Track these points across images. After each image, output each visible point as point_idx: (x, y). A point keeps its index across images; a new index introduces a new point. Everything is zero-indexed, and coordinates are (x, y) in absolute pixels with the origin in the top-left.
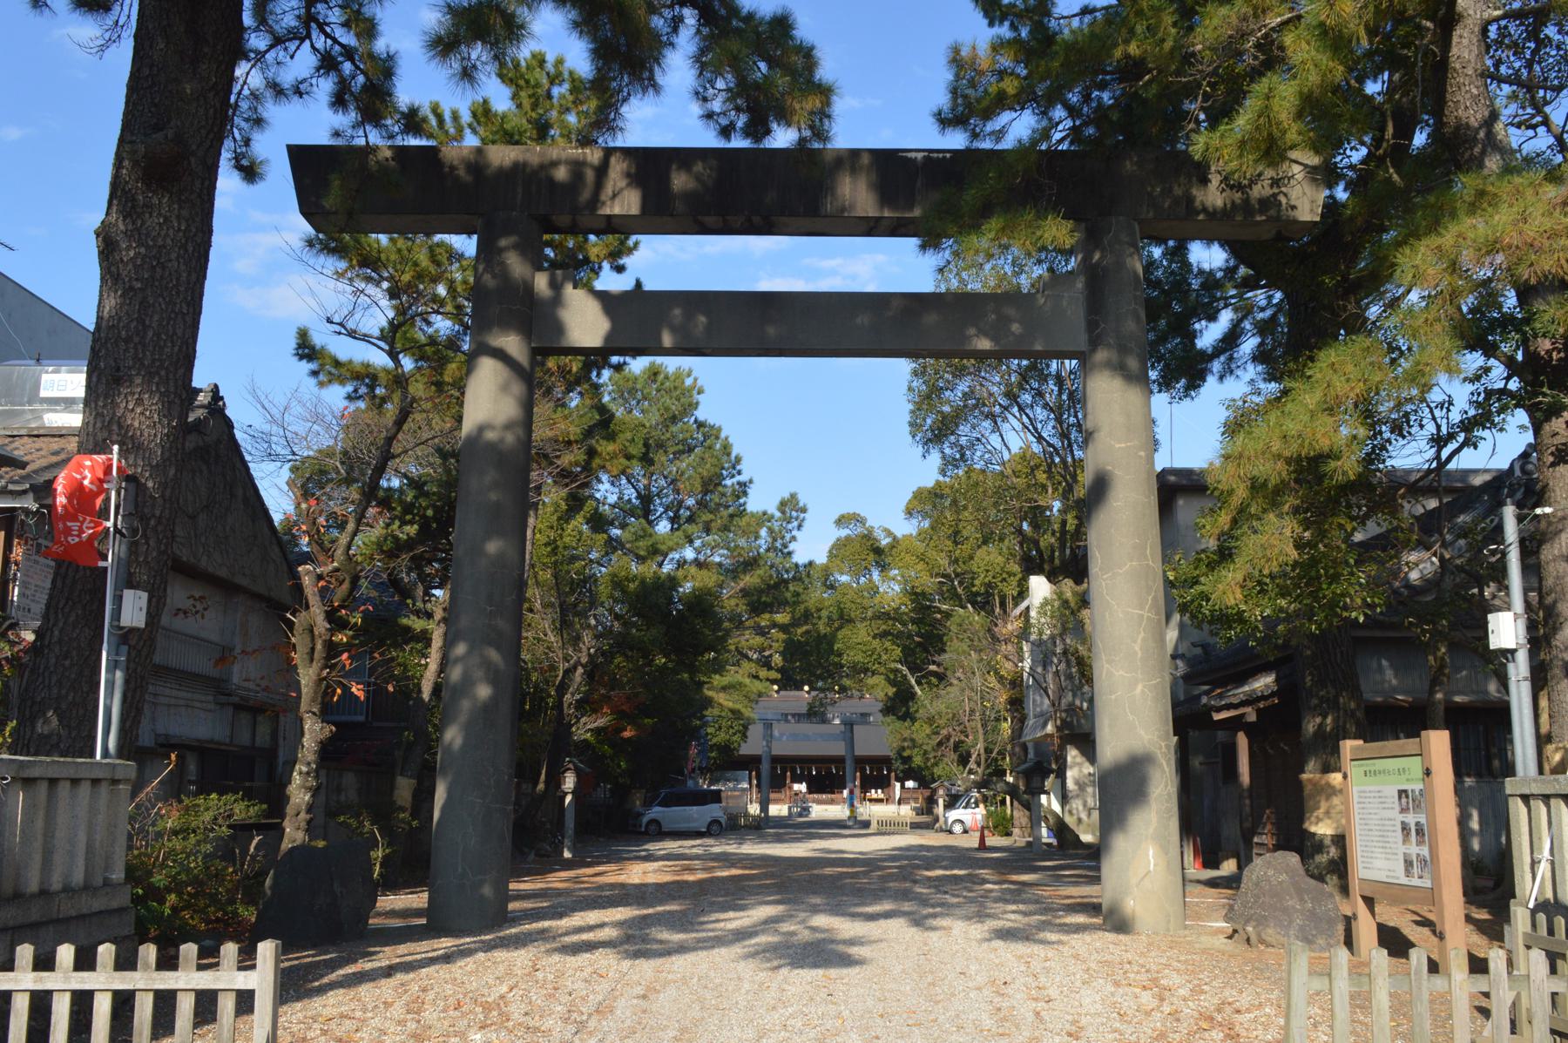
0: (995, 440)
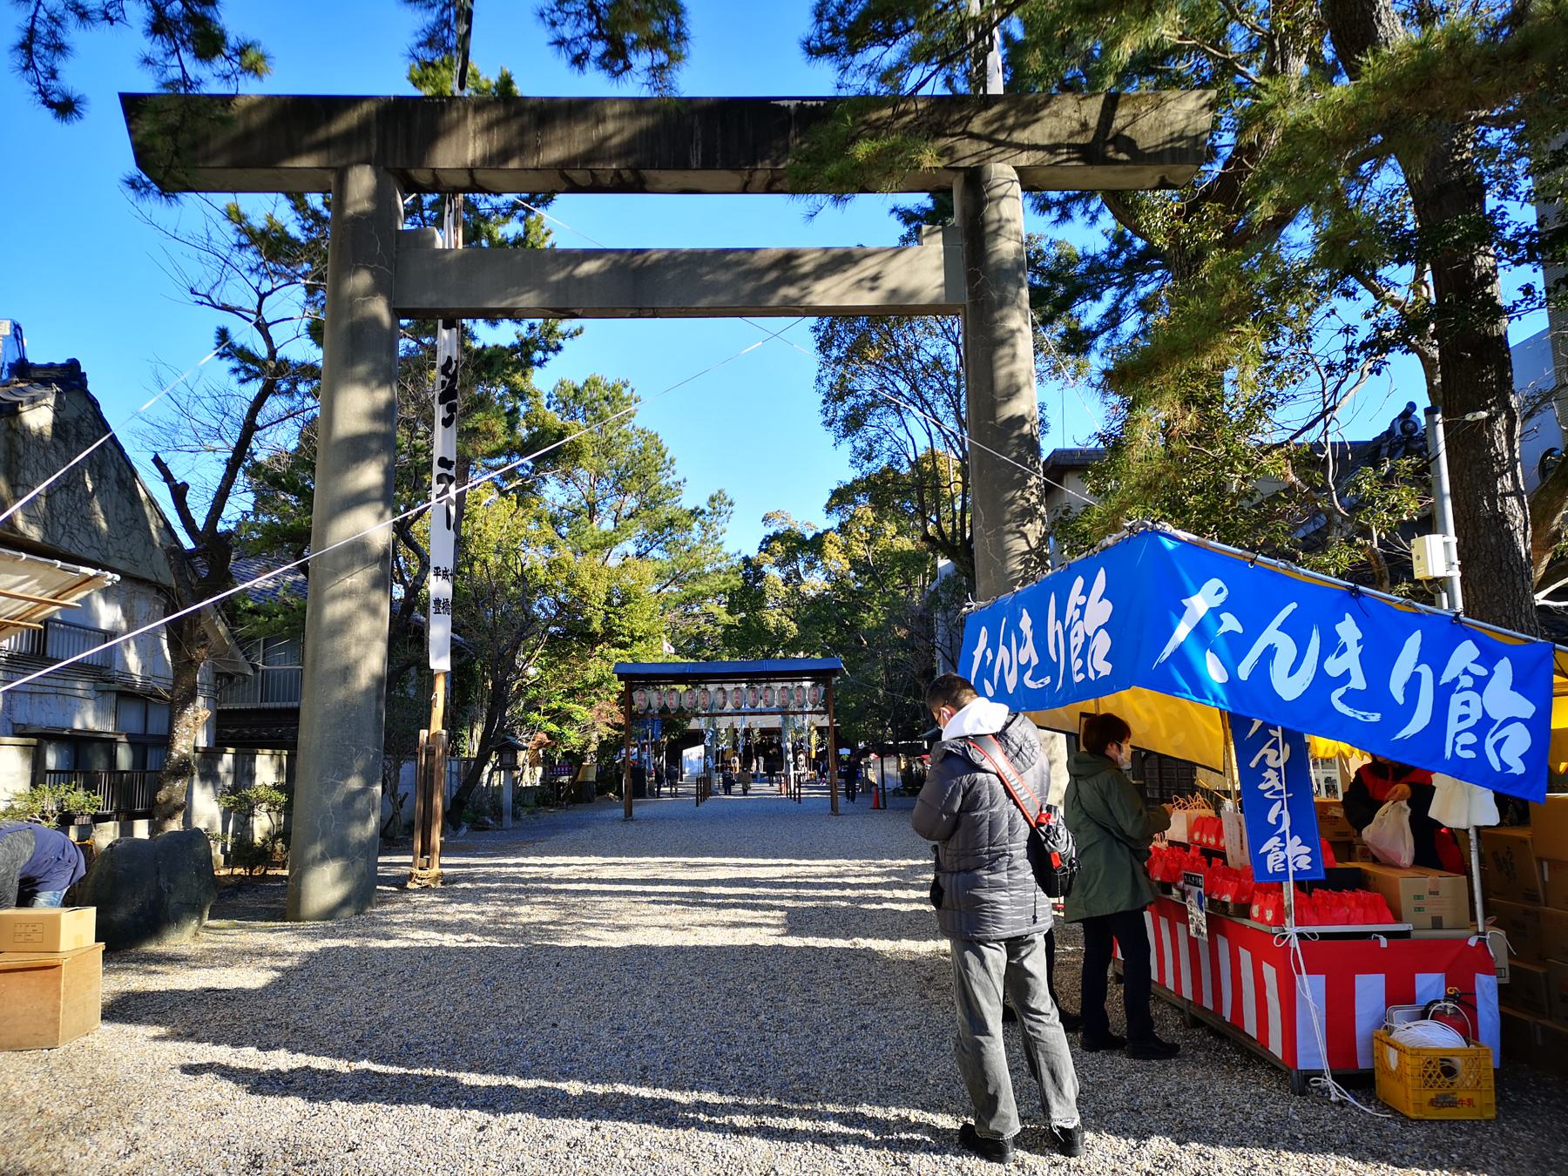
0: (901, 433)
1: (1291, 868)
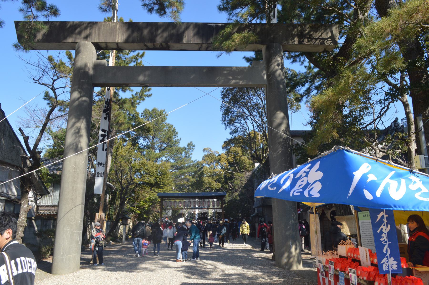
1: (390, 269)
